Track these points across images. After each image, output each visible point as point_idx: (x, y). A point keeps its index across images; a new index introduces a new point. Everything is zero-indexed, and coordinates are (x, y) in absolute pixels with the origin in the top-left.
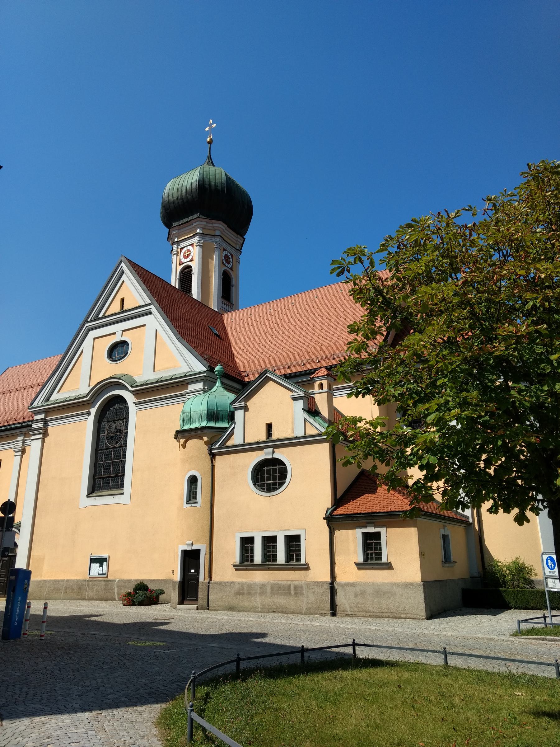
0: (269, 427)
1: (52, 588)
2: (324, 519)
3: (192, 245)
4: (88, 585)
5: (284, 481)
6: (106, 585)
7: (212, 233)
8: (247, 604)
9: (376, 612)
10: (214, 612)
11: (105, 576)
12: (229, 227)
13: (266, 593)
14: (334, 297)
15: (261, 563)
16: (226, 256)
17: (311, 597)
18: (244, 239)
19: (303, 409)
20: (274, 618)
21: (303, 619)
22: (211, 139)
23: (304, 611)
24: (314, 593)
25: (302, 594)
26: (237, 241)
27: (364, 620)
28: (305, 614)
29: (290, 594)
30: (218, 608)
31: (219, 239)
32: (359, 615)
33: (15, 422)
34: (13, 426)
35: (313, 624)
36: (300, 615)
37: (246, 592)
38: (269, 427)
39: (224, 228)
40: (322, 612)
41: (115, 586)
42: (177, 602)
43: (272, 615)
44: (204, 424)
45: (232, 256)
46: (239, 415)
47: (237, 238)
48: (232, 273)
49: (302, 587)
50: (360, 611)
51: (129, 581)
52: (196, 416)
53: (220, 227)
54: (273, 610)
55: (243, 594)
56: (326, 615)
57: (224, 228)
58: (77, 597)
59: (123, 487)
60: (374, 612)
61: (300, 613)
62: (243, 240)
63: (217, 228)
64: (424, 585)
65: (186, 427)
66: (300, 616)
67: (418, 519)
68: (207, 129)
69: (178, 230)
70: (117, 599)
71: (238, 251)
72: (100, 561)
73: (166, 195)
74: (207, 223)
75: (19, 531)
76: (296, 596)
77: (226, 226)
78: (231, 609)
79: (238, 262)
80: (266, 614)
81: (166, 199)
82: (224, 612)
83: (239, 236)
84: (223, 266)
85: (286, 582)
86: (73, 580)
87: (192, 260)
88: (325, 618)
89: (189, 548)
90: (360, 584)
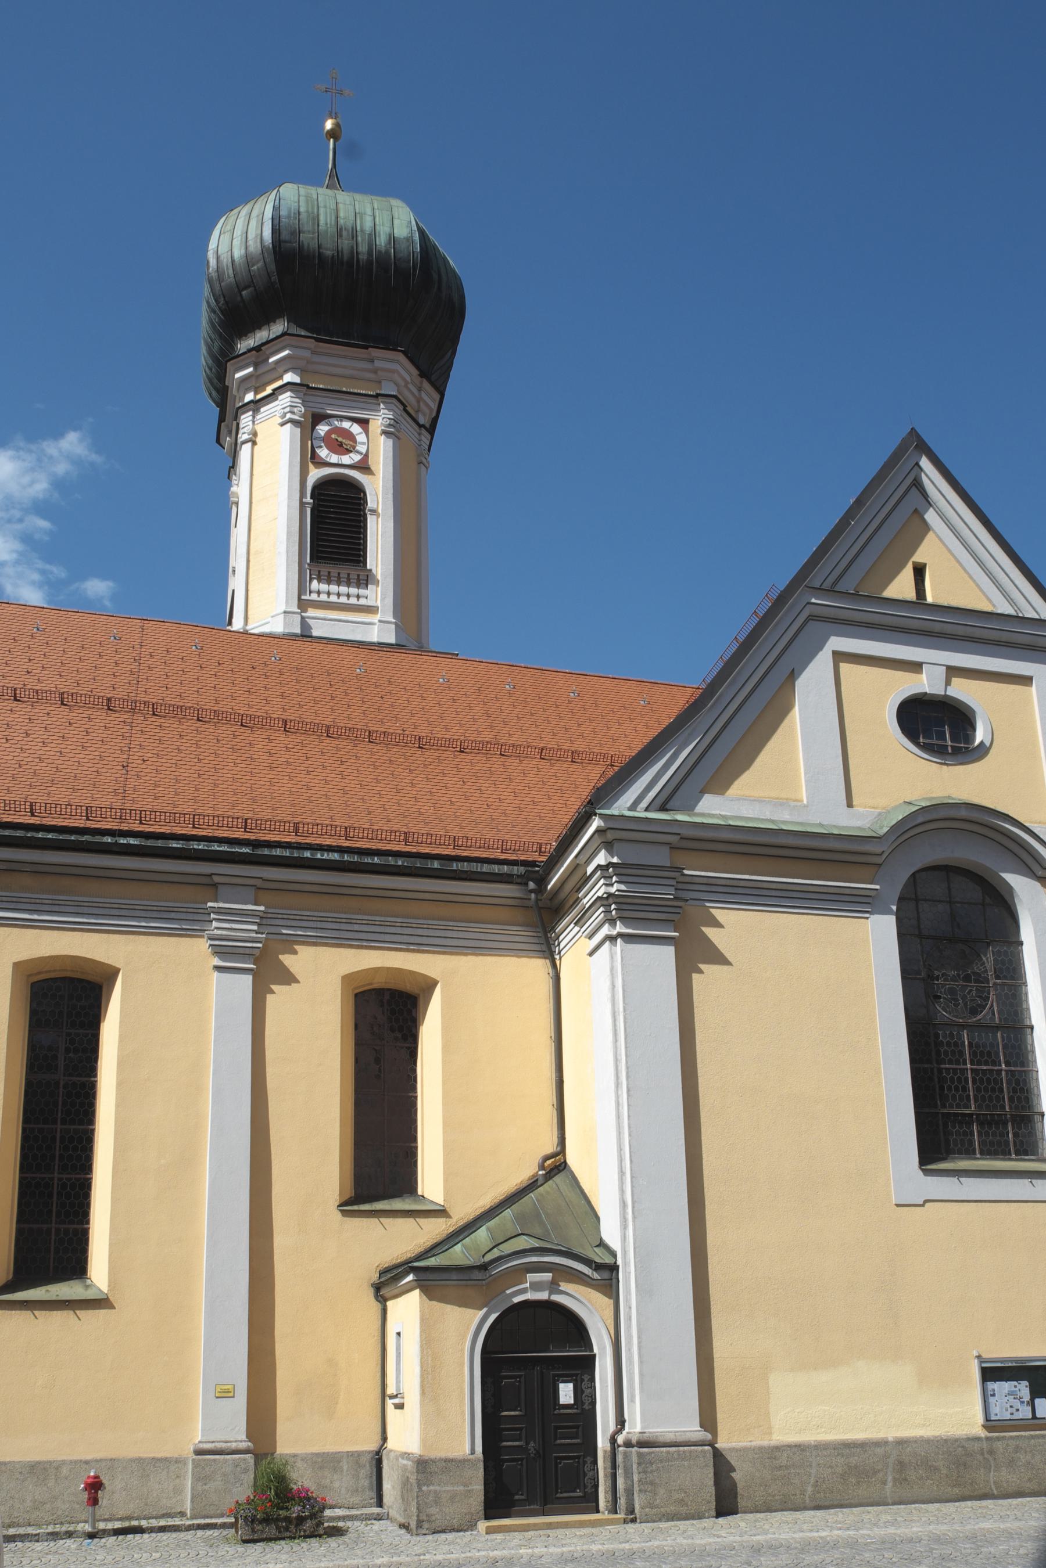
1: (839, 1470)
39: (408, 379)
56: (699, 1516)
57: (408, 379)
58: (956, 1490)
70: (189, 1515)
71: (423, 431)
77: (415, 372)
83: (426, 385)
86: (927, 1441)
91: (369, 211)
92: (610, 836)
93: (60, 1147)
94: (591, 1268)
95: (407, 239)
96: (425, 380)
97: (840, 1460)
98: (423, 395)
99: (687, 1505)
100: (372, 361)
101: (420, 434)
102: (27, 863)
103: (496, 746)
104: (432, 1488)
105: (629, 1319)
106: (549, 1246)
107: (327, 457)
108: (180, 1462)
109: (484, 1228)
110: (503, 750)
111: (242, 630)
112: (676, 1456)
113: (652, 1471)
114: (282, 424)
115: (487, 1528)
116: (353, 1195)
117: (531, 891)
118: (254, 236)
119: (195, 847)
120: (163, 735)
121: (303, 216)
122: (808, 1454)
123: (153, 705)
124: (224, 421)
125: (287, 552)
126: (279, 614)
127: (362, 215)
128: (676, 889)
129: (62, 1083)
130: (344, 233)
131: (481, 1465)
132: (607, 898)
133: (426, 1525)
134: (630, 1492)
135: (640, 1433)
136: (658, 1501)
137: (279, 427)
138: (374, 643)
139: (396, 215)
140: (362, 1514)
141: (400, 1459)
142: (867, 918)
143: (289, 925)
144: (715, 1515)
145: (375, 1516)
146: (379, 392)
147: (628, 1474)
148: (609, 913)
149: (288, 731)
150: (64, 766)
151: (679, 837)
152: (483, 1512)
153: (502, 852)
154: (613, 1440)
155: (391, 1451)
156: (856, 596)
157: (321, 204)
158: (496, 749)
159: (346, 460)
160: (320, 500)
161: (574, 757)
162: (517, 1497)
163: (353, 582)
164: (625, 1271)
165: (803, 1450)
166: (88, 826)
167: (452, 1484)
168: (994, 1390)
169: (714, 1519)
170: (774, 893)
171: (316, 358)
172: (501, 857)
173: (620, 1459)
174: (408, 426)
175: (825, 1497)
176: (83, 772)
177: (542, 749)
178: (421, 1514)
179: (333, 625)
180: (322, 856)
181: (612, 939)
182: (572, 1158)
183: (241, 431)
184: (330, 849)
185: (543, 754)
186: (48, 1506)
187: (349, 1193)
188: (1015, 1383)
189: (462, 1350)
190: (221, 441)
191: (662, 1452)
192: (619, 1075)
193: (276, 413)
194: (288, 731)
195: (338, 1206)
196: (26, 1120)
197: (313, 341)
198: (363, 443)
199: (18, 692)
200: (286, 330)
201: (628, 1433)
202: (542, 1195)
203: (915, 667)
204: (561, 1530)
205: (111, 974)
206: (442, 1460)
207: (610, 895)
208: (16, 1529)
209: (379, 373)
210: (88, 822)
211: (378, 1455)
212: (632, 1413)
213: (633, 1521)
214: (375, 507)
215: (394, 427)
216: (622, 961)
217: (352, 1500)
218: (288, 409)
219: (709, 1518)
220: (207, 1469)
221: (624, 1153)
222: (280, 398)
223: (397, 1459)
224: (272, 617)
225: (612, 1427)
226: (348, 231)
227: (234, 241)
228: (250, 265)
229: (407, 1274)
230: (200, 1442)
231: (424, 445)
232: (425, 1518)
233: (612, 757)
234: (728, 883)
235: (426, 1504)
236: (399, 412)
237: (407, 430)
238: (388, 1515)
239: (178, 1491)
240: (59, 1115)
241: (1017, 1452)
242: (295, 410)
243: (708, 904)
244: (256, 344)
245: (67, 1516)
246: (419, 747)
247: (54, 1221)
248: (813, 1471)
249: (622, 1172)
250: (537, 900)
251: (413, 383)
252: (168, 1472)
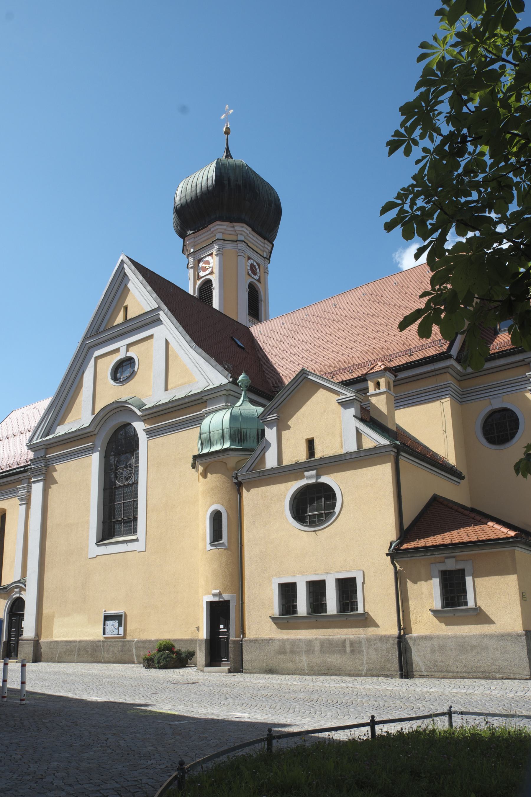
0: (311, 443)
1: (64, 650)
2: (387, 555)
4: (103, 646)
5: (332, 511)
6: (123, 646)
7: (234, 238)
8: (289, 665)
9: (461, 672)
10: (249, 676)
12: (253, 230)
13: (314, 651)
14: (387, 292)
15: (305, 614)
16: (252, 266)
17: (373, 655)
18: (273, 245)
19: (354, 416)
20: (325, 681)
21: (363, 682)
22: (227, 128)
23: (364, 672)
24: (376, 650)
25: (361, 652)
26: (264, 247)
27: (446, 681)
28: (366, 675)
29: (345, 651)
30: (254, 671)
32: (437, 676)
33: (17, 466)
34: (15, 471)
35: (377, 687)
36: (359, 678)
37: (288, 651)
38: (311, 443)
39: (248, 233)
40: (388, 673)
41: (134, 647)
42: (204, 664)
43: (322, 678)
44: (227, 445)
45: (259, 265)
46: (271, 434)
47: (264, 243)
48: (260, 286)
49: (360, 643)
50: (439, 672)
51: (150, 641)
52: (216, 436)
53: (243, 231)
54: (323, 672)
55: (284, 653)
56: (393, 677)
59: (136, 532)
60: (458, 672)
61: (359, 675)
62: (271, 245)
63: (240, 232)
64: (526, 635)
65: (205, 451)
66: (360, 679)
67: (517, 548)
68: (223, 116)
69: (195, 238)
70: (136, 662)
71: (266, 260)
72: (118, 618)
73: (178, 198)
74: (227, 226)
75: (25, 586)
76: (353, 654)
77: (250, 229)
78: (270, 671)
79: (266, 272)
80: (314, 677)
81: (178, 202)
82: (262, 675)
83: (266, 241)
84: (249, 277)
85: (339, 637)
86: (86, 641)
87: (211, 273)
88: (393, 681)
89: (216, 599)
90: (438, 637)
96: (233, 223)
100: (234, 227)
101: (264, 261)
142: (92, 455)
162: (223, 659)
168: (108, 624)
170: (73, 454)
171: (196, 239)
188: (114, 621)
203: (117, 350)
209: (214, 232)
234: (83, 449)
241: (110, 647)
243: (54, 464)
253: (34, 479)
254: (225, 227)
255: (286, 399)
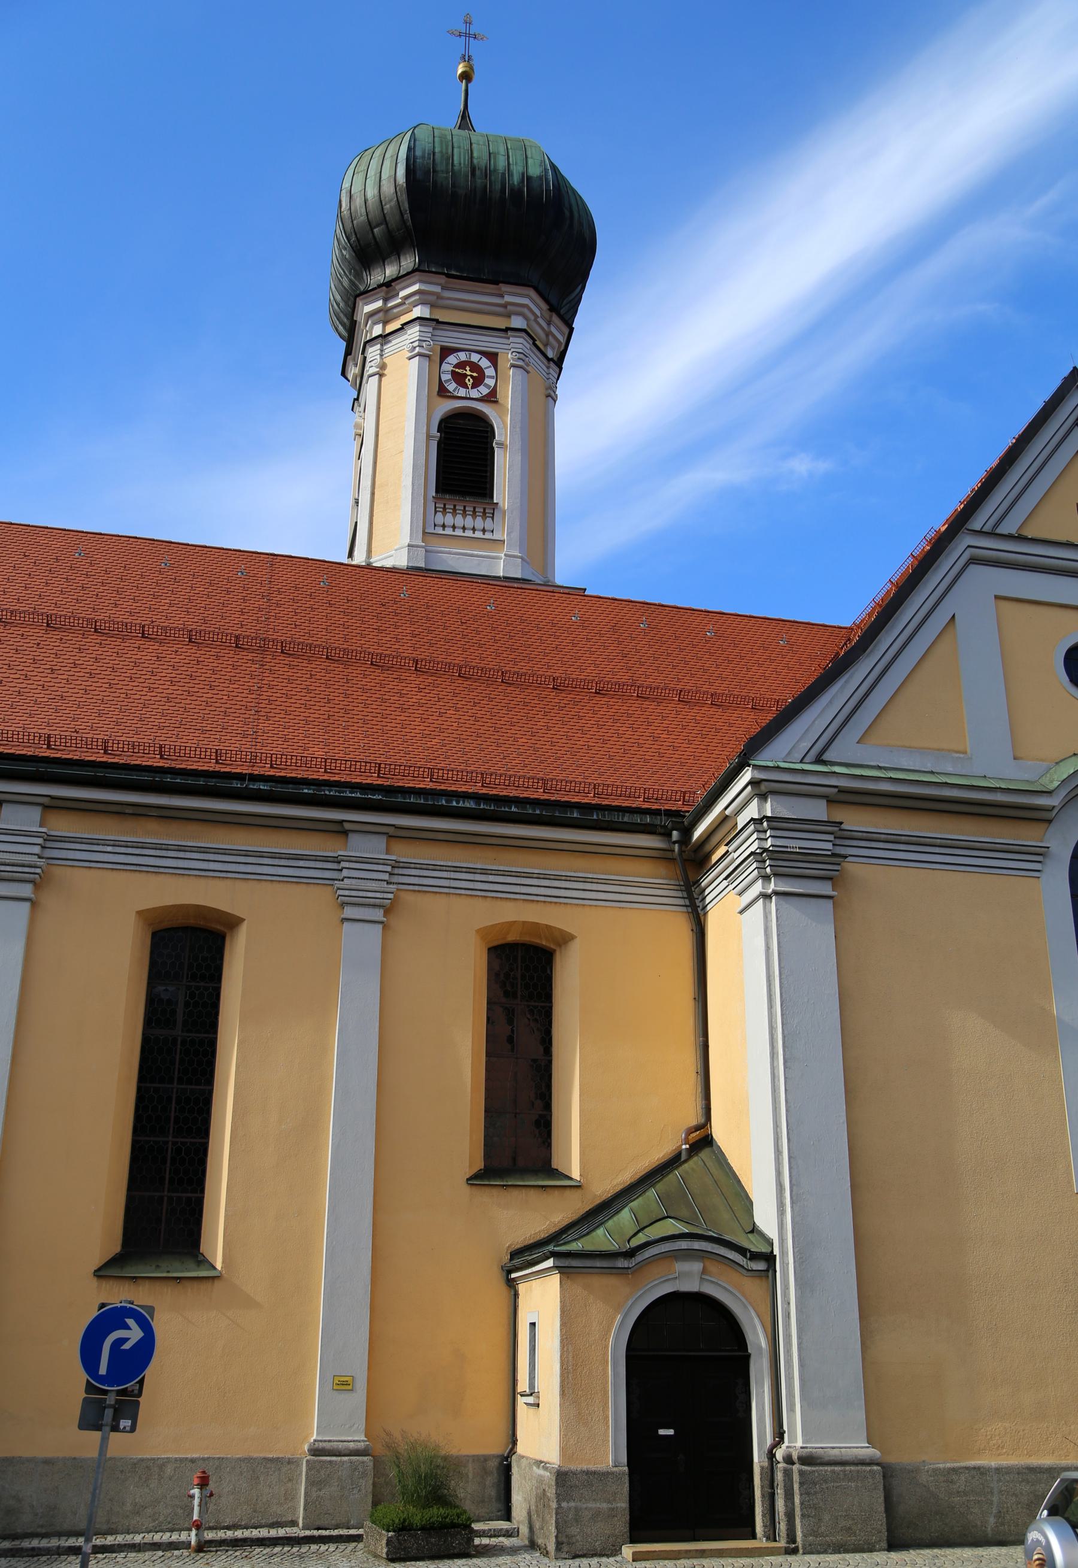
3: (493, 357)
7: (501, 323)
11: (350, 1387)
18: (571, 330)
31: (521, 340)
39: (538, 313)
56: (868, 1548)
57: (538, 313)
70: (301, 1525)
71: (552, 364)
83: (555, 319)
91: (502, 150)
92: (764, 787)
93: (176, 1108)
94: (746, 1257)
95: (540, 178)
97: (1026, 1488)
98: (553, 329)
99: (855, 1533)
100: (502, 296)
101: (548, 368)
102: (154, 807)
103: (633, 688)
104: (572, 1504)
105: (787, 1316)
106: (700, 1232)
107: (454, 390)
108: (293, 1463)
109: (626, 1210)
110: (640, 692)
111: (364, 564)
112: (842, 1476)
113: (816, 1493)
114: (410, 358)
115: (634, 1554)
116: (483, 1167)
117: (675, 842)
118: (387, 176)
119: (327, 793)
120: (292, 674)
121: (438, 156)
122: (988, 1478)
123: (282, 643)
124: (350, 354)
125: (413, 484)
126: (402, 548)
127: (496, 154)
128: (834, 845)
129: (179, 1039)
130: (478, 173)
131: (626, 1479)
132: (761, 854)
133: (565, 1548)
134: (790, 1516)
135: (802, 1448)
136: (823, 1528)
137: (408, 361)
138: (499, 577)
139: (529, 155)
140: (490, 1530)
141: (535, 1468)
143: (421, 874)
144: (886, 1548)
145: (503, 1533)
146: (508, 326)
147: (789, 1496)
148: (763, 870)
149: (419, 671)
150: (192, 706)
151: (836, 790)
152: (628, 1534)
153: (644, 801)
154: (771, 1455)
155: (523, 1457)
156: (1020, 538)
157: (455, 145)
158: (632, 691)
159: (474, 393)
160: (446, 433)
161: (717, 701)
163: (460, 514)
164: (783, 1262)
165: (982, 1474)
166: (217, 769)
167: (594, 1500)
169: (886, 1552)
171: (447, 294)
172: (644, 807)
173: (779, 1476)
174: (536, 359)
175: (1010, 1530)
176: (211, 713)
177: (681, 691)
178: (560, 1535)
179: (458, 559)
180: (458, 802)
181: (766, 897)
182: (719, 1131)
183: (368, 365)
184: (466, 796)
185: (682, 697)
186: (149, 1511)
187: (480, 1165)
189: (606, 1347)
190: (346, 374)
191: (826, 1471)
192: (775, 1044)
193: (405, 347)
194: (419, 671)
195: (468, 1180)
196: (142, 1078)
197: (444, 276)
198: (492, 377)
199: (146, 629)
200: (417, 266)
201: (788, 1447)
202: (687, 1173)
204: (716, 1559)
205: (233, 923)
206: (584, 1472)
207: (765, 850)
208: (114, 1536)
209: (509, 307)
210: (217, 765)
211: (507, 1461)
212: (792, 1424)
213: (794, 1551)
214: (503, 440)
215: (523, 361)
216: (777, 921)
217: (477, 1512)
218: (416, 344)
219: (879, 1550)
220: (322, 1473)
221: (781, 1129)
222: (409, 332)
223: (531, 1468)
224: (396, 550)
225: (769, 1441)
226: (481, 170)
227: (368, 180)
228: (383, 204)
229: (547, 1258)
230: (315, 1441)
231: (553, 378)
232: (564, 1539)
233: (753, 699)
235: (566, 1522)
236: (528, 346)
237: (537, 365)
238: (518, 1532)
239: (290, 1496)
240: (176, 1073)
242: (424, 344)
244: (386, 280)
245: (169, 1523)
246: (554, 688)
247: (166, 1190)
248: (995, 1499)
249: (778, 1151)
250: (681, 851)
251: (542, 317)
252: (279, 1474)
253: (360, 794)
254: (437, 289)
255: (860, 688)
